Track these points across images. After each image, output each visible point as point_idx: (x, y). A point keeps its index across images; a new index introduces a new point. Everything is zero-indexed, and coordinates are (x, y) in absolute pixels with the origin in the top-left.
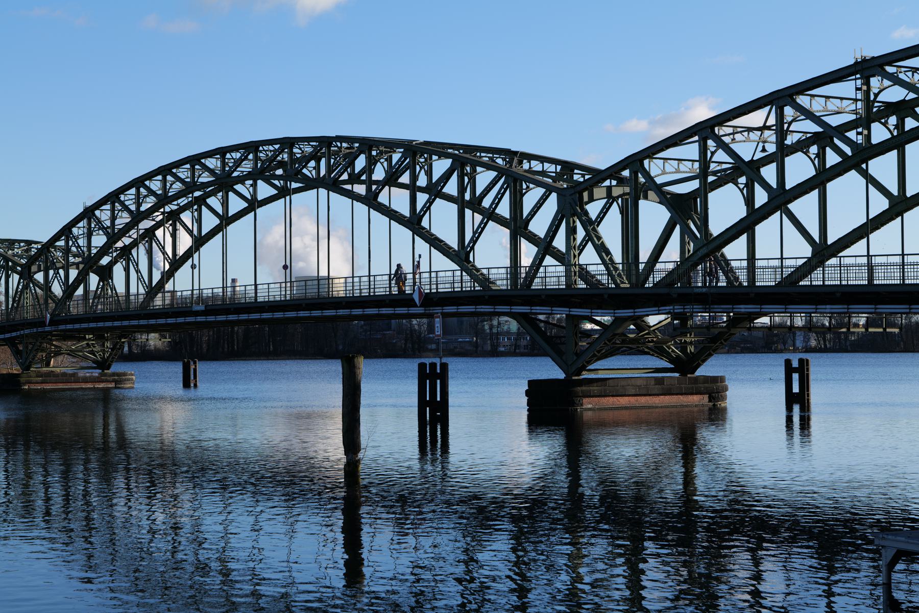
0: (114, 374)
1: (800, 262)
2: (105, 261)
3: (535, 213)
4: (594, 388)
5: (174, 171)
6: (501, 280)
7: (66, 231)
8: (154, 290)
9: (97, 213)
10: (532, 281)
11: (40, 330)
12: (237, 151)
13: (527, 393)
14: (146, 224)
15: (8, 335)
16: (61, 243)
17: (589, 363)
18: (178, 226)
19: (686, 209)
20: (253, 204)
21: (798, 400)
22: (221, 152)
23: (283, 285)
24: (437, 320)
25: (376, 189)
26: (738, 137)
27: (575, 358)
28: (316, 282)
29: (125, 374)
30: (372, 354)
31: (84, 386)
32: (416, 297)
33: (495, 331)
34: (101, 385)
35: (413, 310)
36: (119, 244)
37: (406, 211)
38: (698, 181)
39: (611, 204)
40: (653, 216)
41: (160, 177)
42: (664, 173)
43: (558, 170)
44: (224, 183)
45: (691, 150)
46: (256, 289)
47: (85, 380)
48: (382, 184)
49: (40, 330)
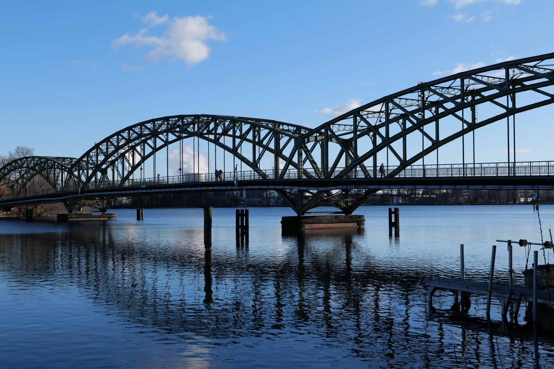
0: (108, 214)
1: (395, 168)
2: (104, 166)
4: (310, 220)
6: (271, 175)
7: (87, 154)
10: (284, 176)
13: (282, 222)
14: (122, 151)
15: (62, 198)
17: (307, 209)
19: (348, 146)
20: (167, 143)
21: (394, 225)
22: (153, 121)
26: (370, 116)
29: (112, 214)
30: (216, 206)
31: (95, 219)
33: (268, 196)
34: (102, 219)
35: (234, 188)
36: (110, 160)
40: (334, 148)
41: (127, 131)
42: (339, 130)
44: (155, 134)
45: (350, 121)
47: (95, 217)
48: (221, 135)
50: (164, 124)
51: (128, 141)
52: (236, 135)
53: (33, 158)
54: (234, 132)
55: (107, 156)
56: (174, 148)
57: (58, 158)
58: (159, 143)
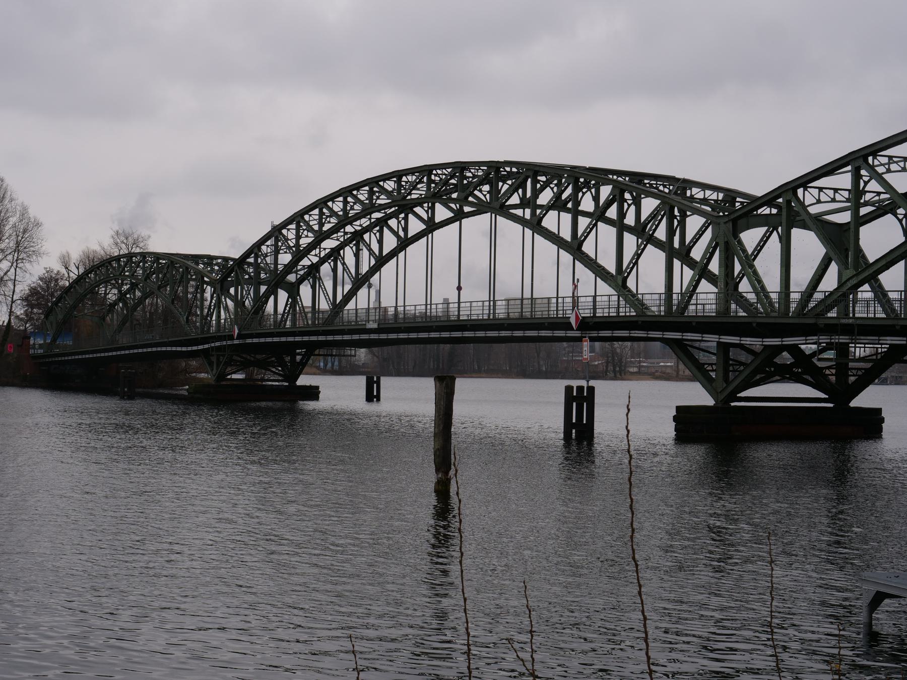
2: (292, 278)
3: (698, 240)
5: (355, 192)
7: (255, 249)
8: (338, 307)
9: (284, 231)
10: (686, 307)
11: (229, 343)
12: (413, 174)
13: (675, 419)
14: (329, 244)
16: (251, 260)
18: (362, 246)
19: (840, 241)
20: (432, 226)
22: (398, 175)
23: (487, 304)
24: (585, 343)
25: (541, 213)
26: (894, 167)
27: (725, 385)
28: (519, 302)
32: (573, 321)
35: (570, 334)
36: (305, 262)
37: (566, 234)
38: (849, 212)
39: (772, 233)
40: (808, 247)
41: (341, 199)
42: (819, 201)
43: (720, 198)
44: (405, 207)
45: (843, 180)
46: (459, 307)
49: (229, 343)
50: (421, 182)
51: (345, 220)
52: (626, 221)
53: (144, 255)
54: (622, 214)
55: (299, 254)
56: (445, 237)
57: (196, 258)
58: (415, 226)
